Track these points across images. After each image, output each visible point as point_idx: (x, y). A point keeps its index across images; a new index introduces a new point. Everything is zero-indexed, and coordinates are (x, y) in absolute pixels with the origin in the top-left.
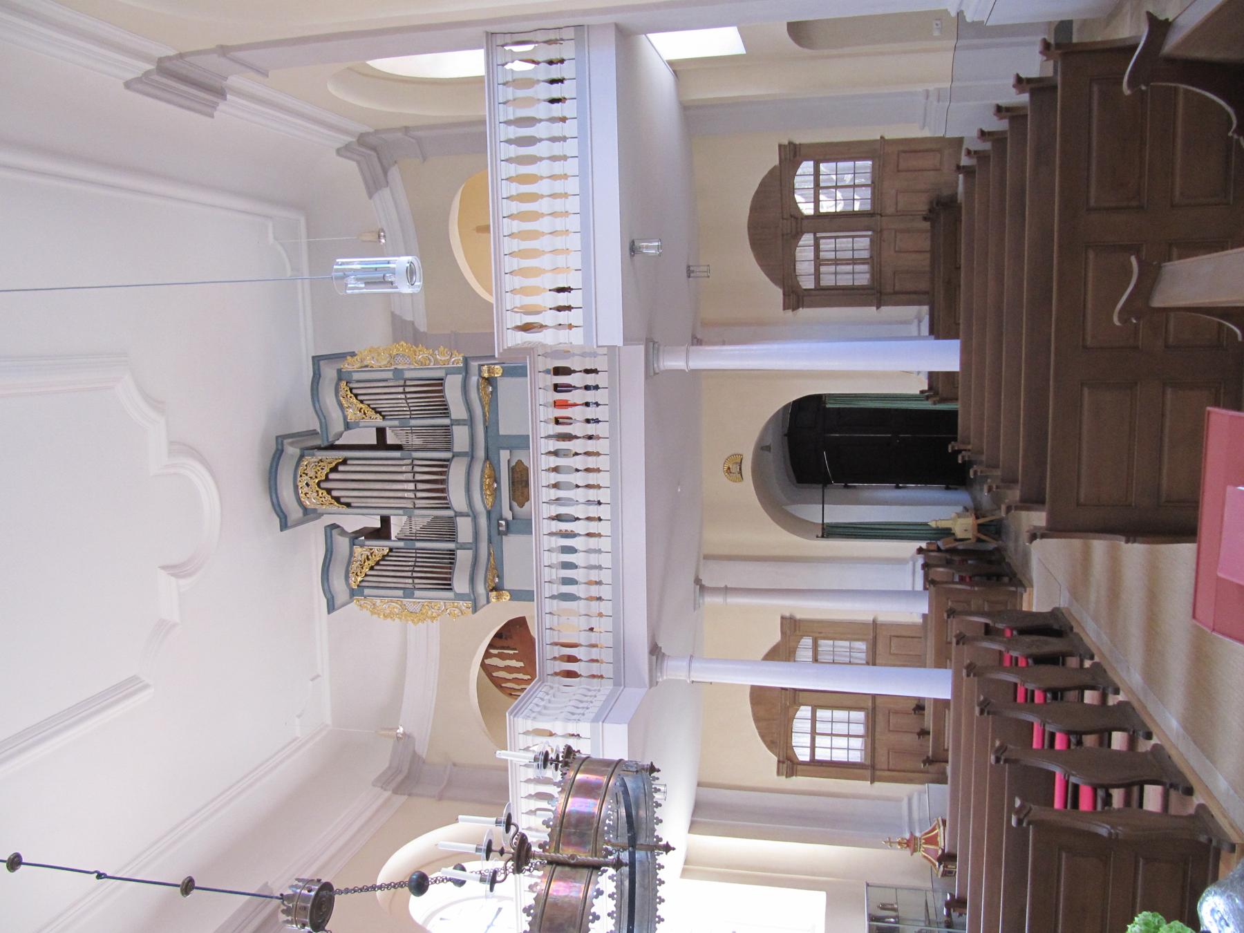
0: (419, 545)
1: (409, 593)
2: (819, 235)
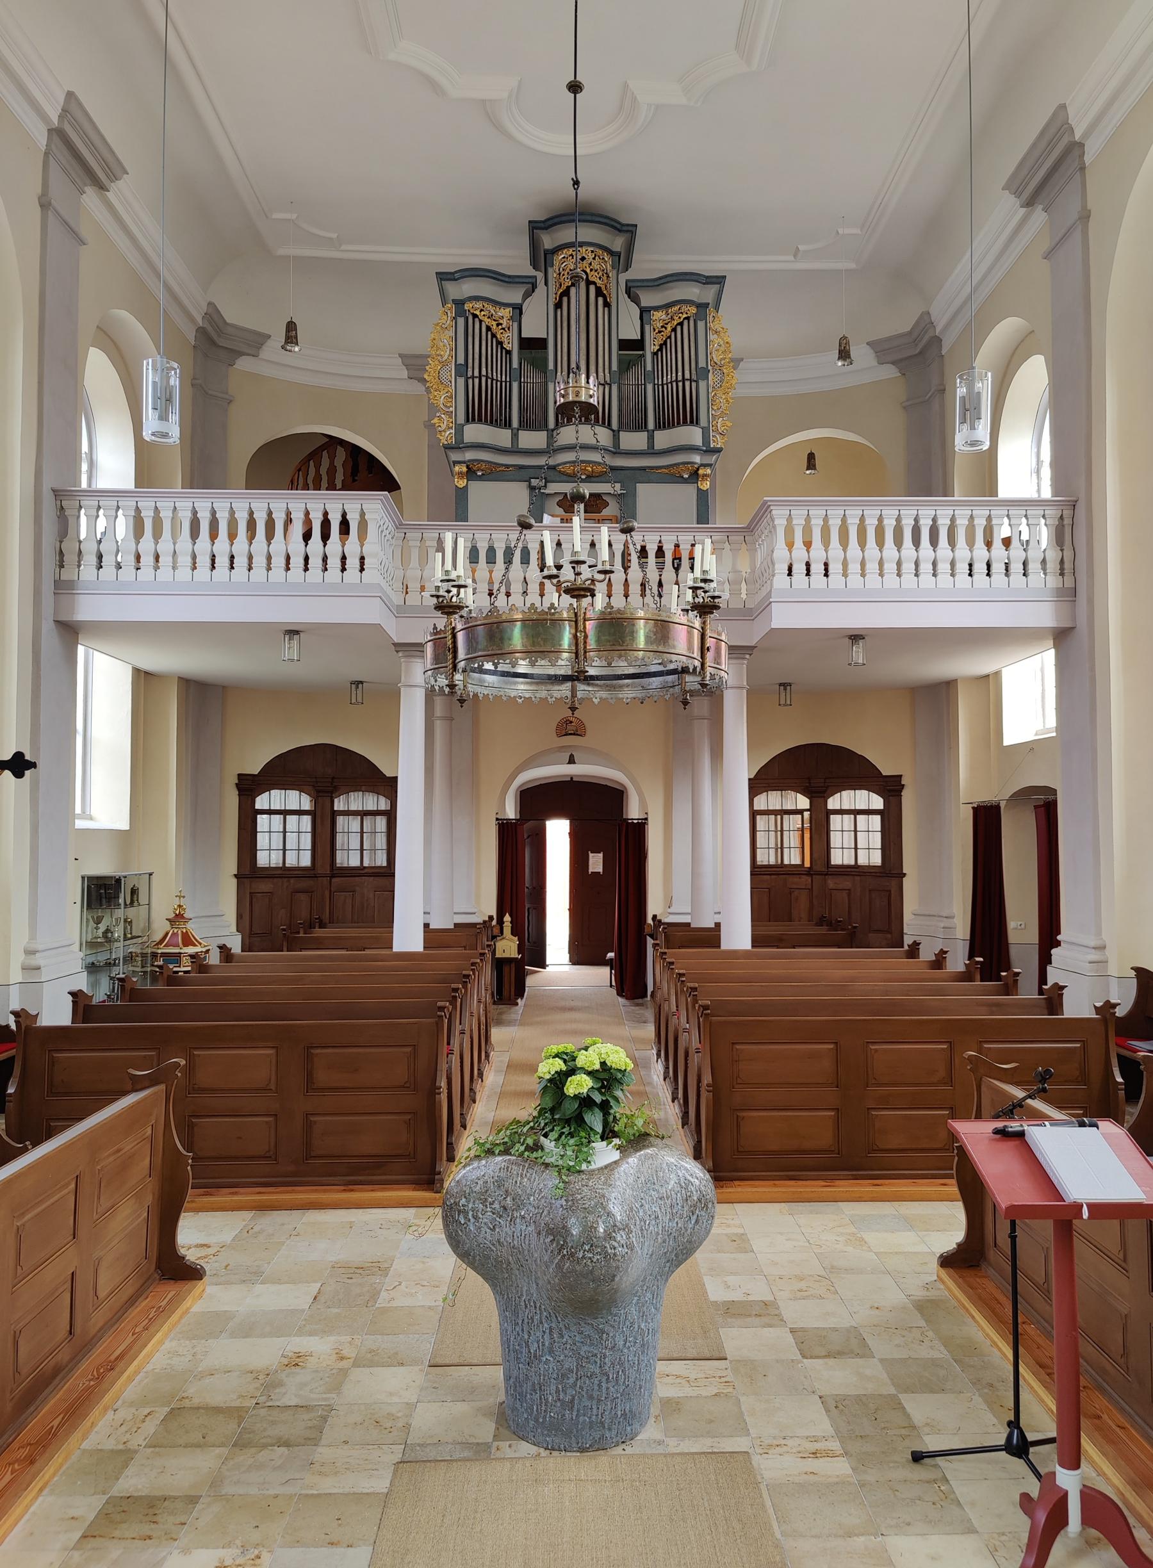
0: (515, 385)
1: (461, 370)
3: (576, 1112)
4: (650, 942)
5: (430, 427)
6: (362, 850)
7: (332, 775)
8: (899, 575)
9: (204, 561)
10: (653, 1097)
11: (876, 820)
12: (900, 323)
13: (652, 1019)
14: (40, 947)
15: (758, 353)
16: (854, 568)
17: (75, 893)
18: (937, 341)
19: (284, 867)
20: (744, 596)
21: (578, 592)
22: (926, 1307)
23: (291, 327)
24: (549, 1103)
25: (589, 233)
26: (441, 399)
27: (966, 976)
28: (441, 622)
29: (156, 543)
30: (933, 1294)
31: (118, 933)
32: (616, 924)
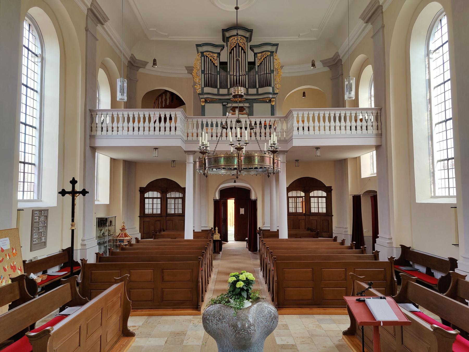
0: (218, 76)
1: (203, 72)
2: (304, 198)
3: (239, 292)
4: (258, 235)
5: (195, 89)
6: (175, 209)
7: (166, 187)
8: (330, 130)
9: (131, 129)
10: (261, 286)
11: (324, 199)
12: (330, 55)
13: (259, 258)
14: (86, 239)
15: (288, 65)
16: (317, 128)
17: (94, 223)
18: (340, 60)
19: (153, 214)
20: (285, 136)
21: (239, 149)
22: (339, 347)
23: (155, 60)
24: (232, 289)
25: (241, 32)
26: (197, 80)
27: (351, 248)
28: (201, 155)
29: (118, 124)
30: (341, 343)
31: (106, 234)
32: (248, 227)
